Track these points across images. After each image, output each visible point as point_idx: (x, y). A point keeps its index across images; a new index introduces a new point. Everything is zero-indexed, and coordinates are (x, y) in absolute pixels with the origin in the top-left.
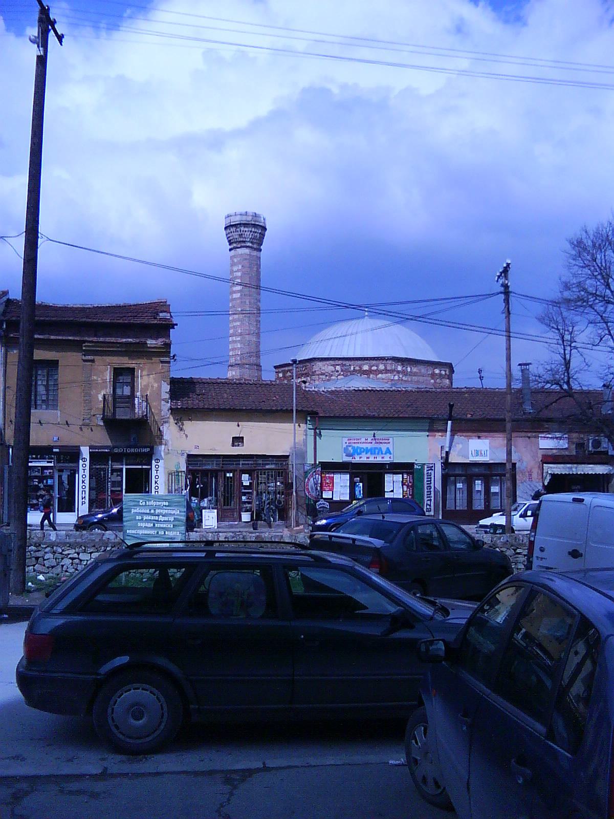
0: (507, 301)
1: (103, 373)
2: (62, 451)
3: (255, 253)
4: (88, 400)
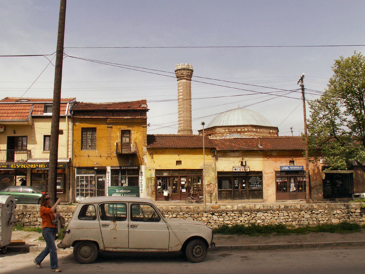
0: (303, 93)
1: (116, 132)
2: (98, 169)
3: (189, 81)
4: (110, 146)
